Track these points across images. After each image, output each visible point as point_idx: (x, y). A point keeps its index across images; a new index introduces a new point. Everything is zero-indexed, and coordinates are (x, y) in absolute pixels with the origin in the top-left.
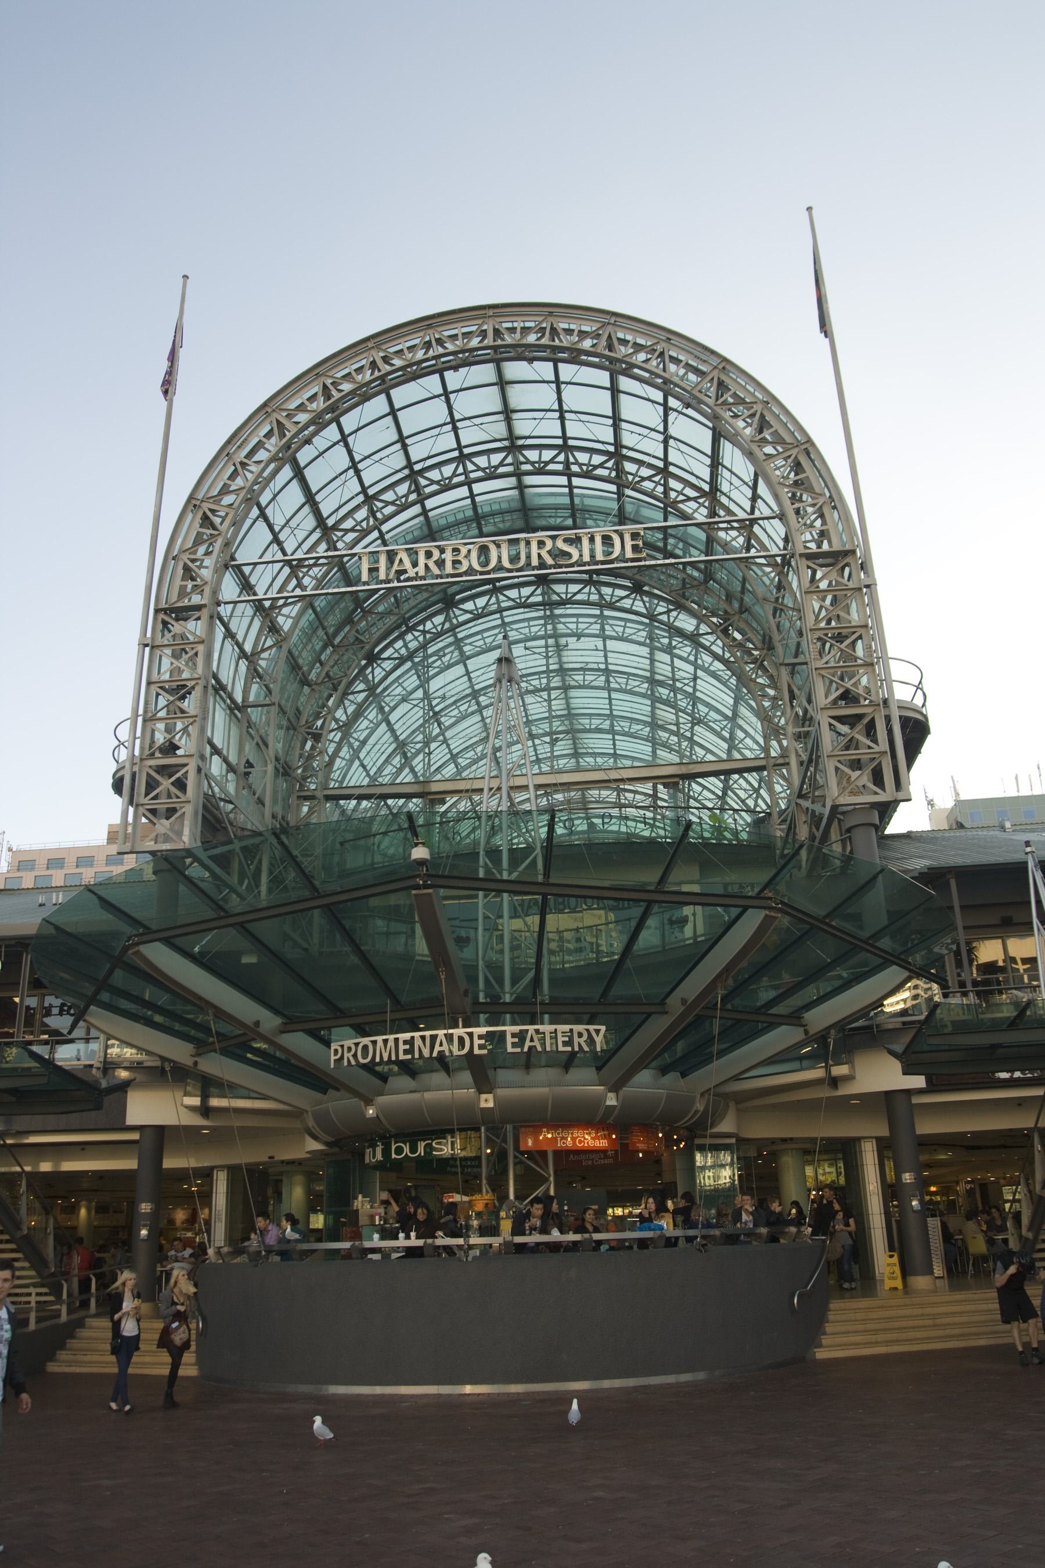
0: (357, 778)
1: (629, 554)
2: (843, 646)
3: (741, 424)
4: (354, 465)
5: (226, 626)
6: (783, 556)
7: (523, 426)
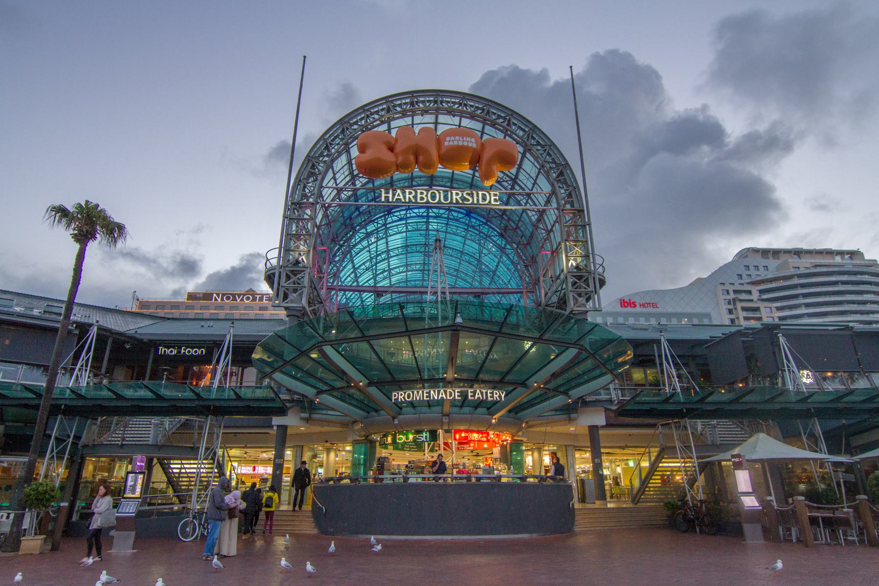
3: (562, 191)
5: (334, 174)
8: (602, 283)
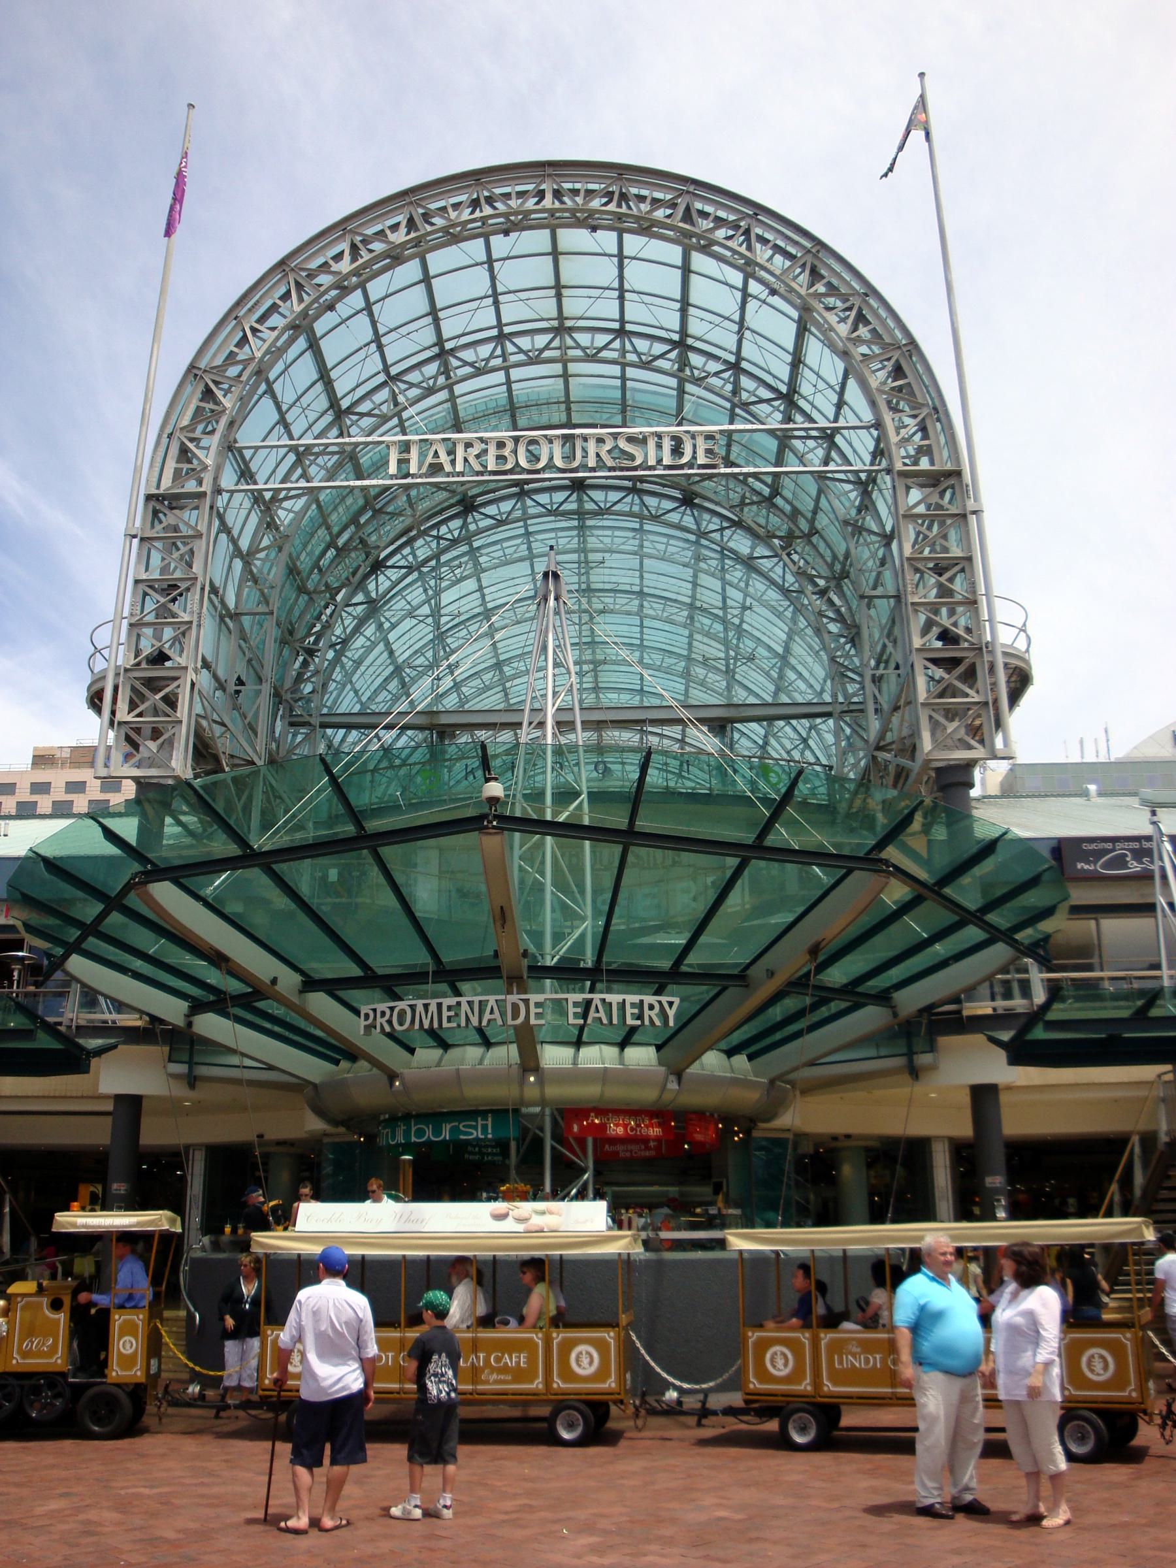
0: (348, 704)
1: (702, 460)
2: (942, 579)
4: (377, 339)
6: (869, 472)
7: (574, 306)
8: (1020, 681)
